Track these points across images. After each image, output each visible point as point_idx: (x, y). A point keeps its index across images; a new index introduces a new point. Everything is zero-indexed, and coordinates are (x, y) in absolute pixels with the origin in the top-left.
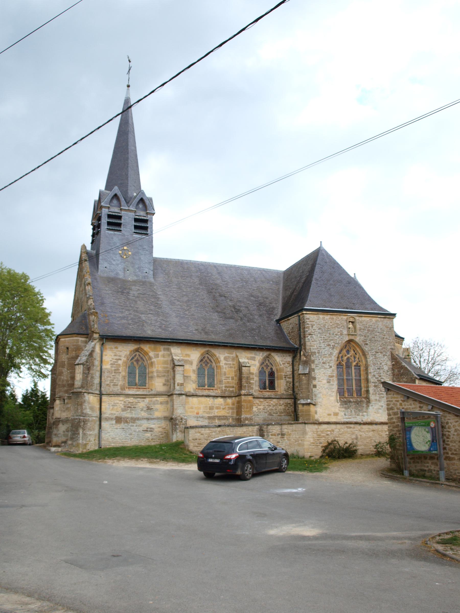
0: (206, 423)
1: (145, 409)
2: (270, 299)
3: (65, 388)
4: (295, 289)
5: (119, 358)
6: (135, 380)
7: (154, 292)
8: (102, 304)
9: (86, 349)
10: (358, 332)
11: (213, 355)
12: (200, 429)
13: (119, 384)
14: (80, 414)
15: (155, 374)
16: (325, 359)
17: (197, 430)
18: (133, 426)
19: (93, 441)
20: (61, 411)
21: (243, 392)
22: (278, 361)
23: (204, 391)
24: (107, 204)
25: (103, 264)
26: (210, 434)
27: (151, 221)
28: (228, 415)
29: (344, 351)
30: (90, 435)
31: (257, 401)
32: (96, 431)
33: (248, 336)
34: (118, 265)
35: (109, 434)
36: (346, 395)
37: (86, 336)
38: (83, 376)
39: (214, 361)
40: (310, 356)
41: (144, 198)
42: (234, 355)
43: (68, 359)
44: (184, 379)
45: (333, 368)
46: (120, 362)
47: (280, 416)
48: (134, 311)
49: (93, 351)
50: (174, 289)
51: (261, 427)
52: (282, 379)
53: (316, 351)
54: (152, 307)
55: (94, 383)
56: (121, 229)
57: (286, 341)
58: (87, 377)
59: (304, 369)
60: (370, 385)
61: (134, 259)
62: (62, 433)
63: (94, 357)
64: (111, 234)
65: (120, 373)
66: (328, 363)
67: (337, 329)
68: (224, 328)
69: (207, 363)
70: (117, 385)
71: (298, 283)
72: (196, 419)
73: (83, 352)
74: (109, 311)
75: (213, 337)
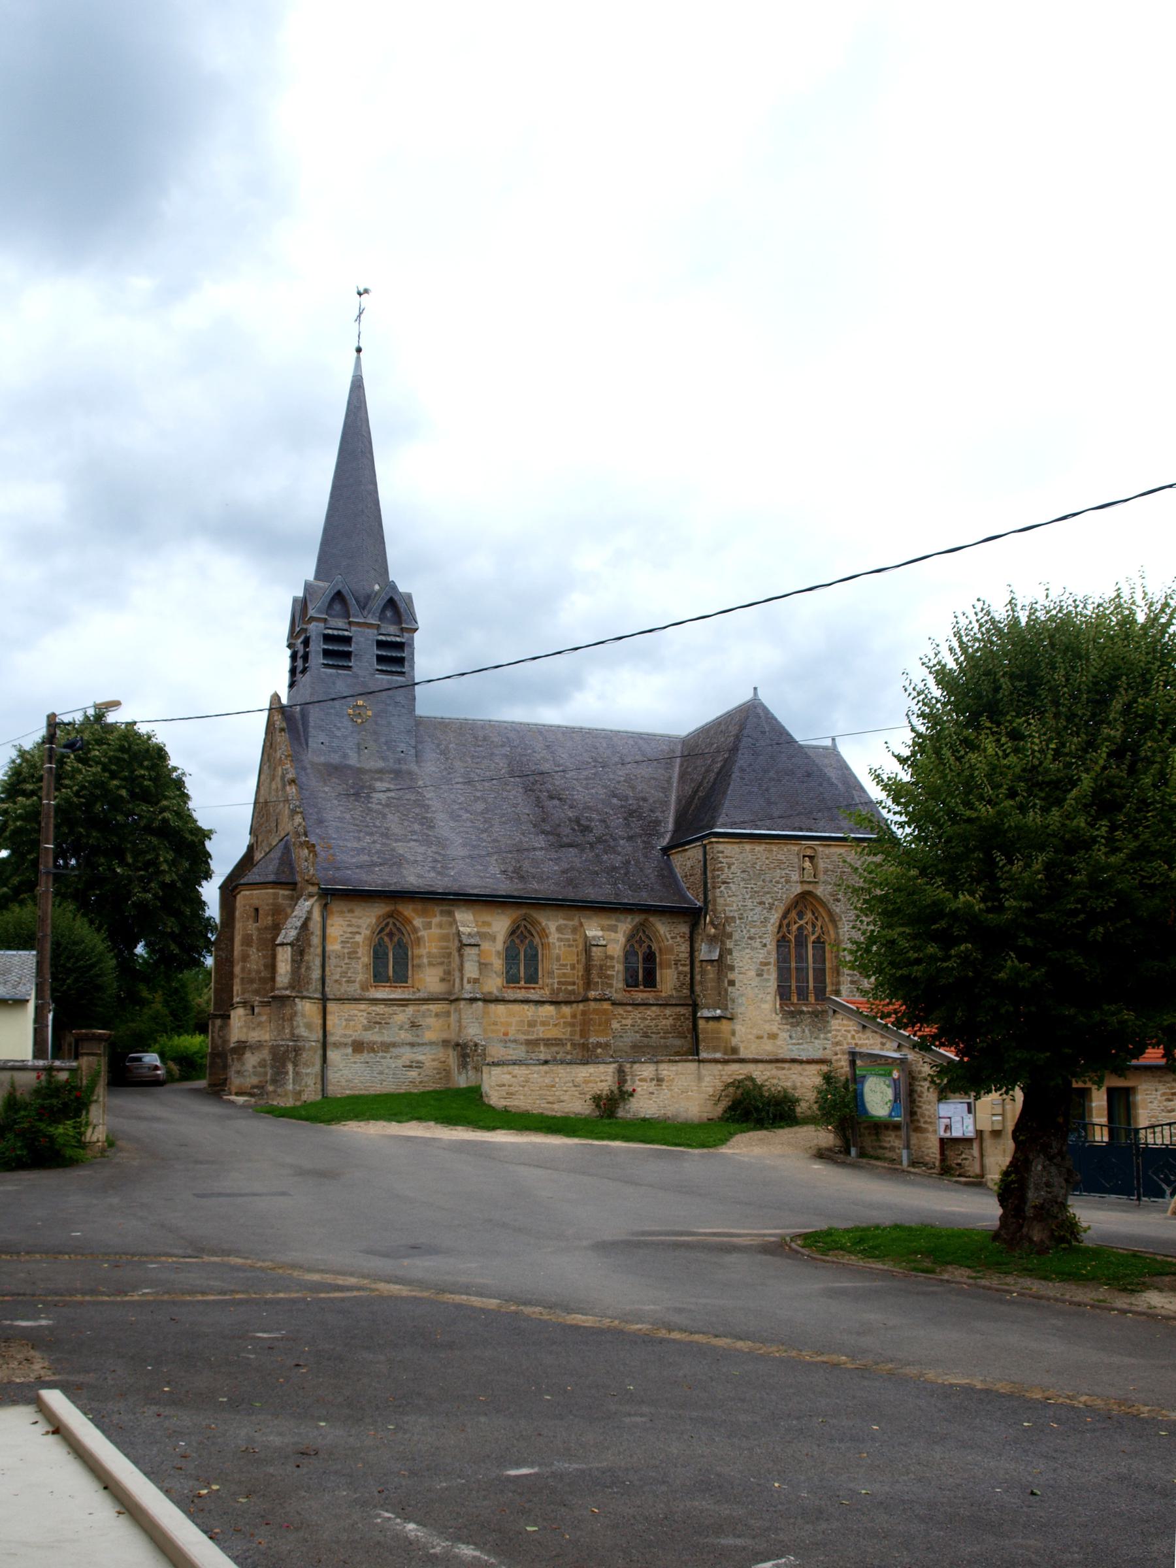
0: (519, 1052)
1: (407, 1027)
3: (255, 986)
4: (701, 784)
6: (388, 972)
7: (419, 792)
8: (320, 822)
9: (294, 914)
11: (534, 923)
12: (510, 1068)
13: (358, 979)
16: (753, 930)
18: (385, 1058)
19: (312, 1085)
20: (249, 1027)
21: (592, 994)
22: (662, 932)
23: (518, 991)
25: (317, 738)
27: (411, 645)
30: (307, 1074)
31: (620, 1010)
33: (605, 884)
34: (345, 737)
36: (795, 999)
37: (291, 887)
38: (292, 966)
39: (538, 933)
40: (724, 925)
41: (396, 598)
42: (575, 922)
43: (258, 929)
45: (769, 946)
46: (359, 938)
48: (382, 835)
50: (459, 786)
51: (620, 1066)
52: (670, 967)
53: (736, 915)
54: (416, 827)
56: (350, 664)
57: (679, 892)
58: (299, 968)
59: (710, 951)
60: (842, 979)
61: (377, 724)
63: (311, 930)
64: (331, 674)
65: (359, 958)
66: (760, 937)
68: (556, 868)
69: (523, 938)
73: (290, 920)
74: (334, 836)
75: (536, 886)
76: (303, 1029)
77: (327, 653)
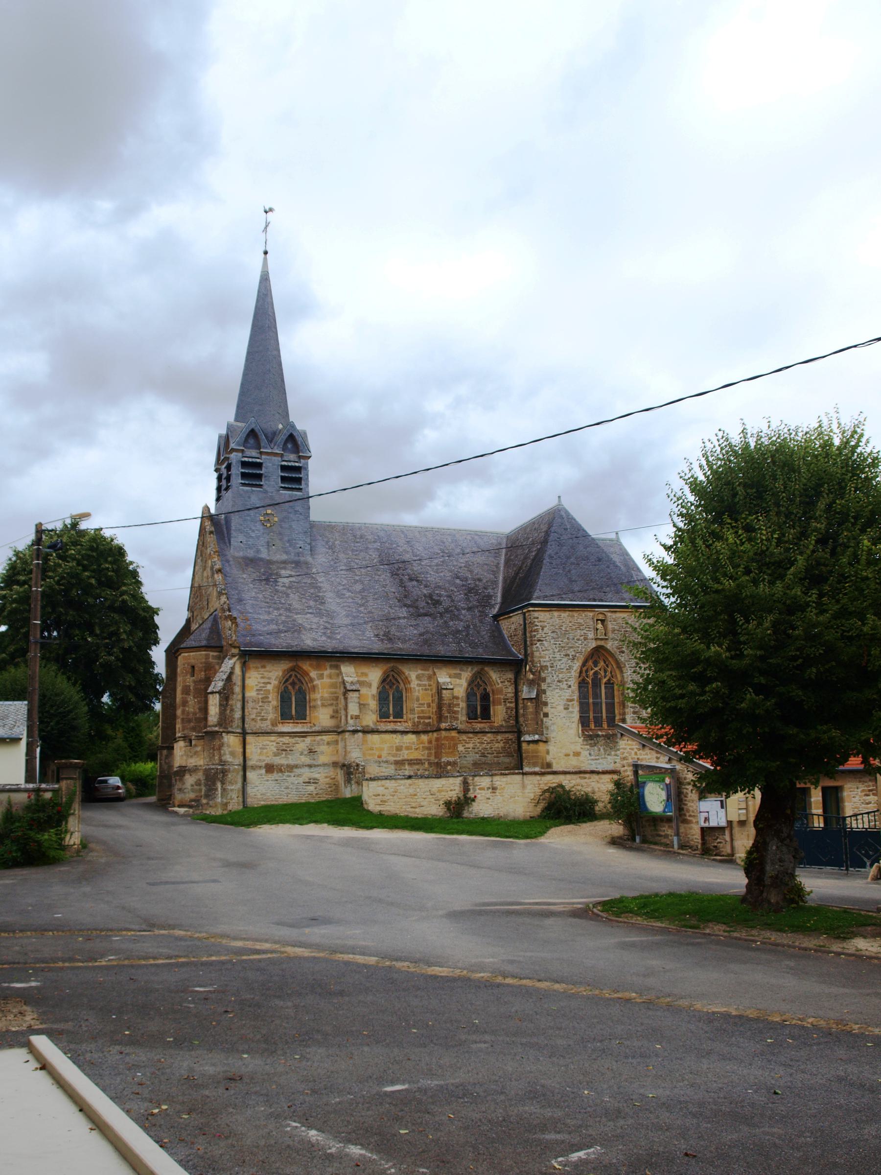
0: (390, 770)
1: (306, 753)
2: (484, 581)
3: (192, 724)
4: (521, 568)
5: (267, 681)
7: (313, 577)
8: (240, 600)
9: (221, 669)
10: (611, 635)
11: (400, 673)
12: (384, 782)
13: (269, 718)
14: (217, 762)
15: (319, 703)
16: (561, 676)
17: (380, 783)
18: (290, 776)
21: (443, 725)
22: (494, 678)
23: (388, 724)
24: (239, 445)
25: (237, 539)
26: (398, 788)
27: (306, 469)
28: (422, 758)
29: (590, 663)
30: (232, 790)
31: (464, 737)
32: (239, 785)
33: (451, 643)
35: (256, 789)
36: (592, 726)
38: (220, 709)
39: (403, 681)
40: (540, 672)
42: (430, 672)
43: (194, 682)
44: (360, 709)
45: (572, 687)
46: (269, 687)
47: (497, 757)
48: (286, 609)
49: (231, 674)
50: (343, 572)
53: (548, 664)
54: (312, 603)
55: (234, 718)
58: (225, 710)
62: (190, 787)
64: (247, 491)
65: (270, 702)
66: (566, 681)
67: (579, 631)
68: (415, 632)
69: (391, 685)
70: (266, 720)
71: (526, 558)
72: (377, 764)
74: (250, 611)
75: (400, 646)
76: (228, 756)
77: (244, 475)
